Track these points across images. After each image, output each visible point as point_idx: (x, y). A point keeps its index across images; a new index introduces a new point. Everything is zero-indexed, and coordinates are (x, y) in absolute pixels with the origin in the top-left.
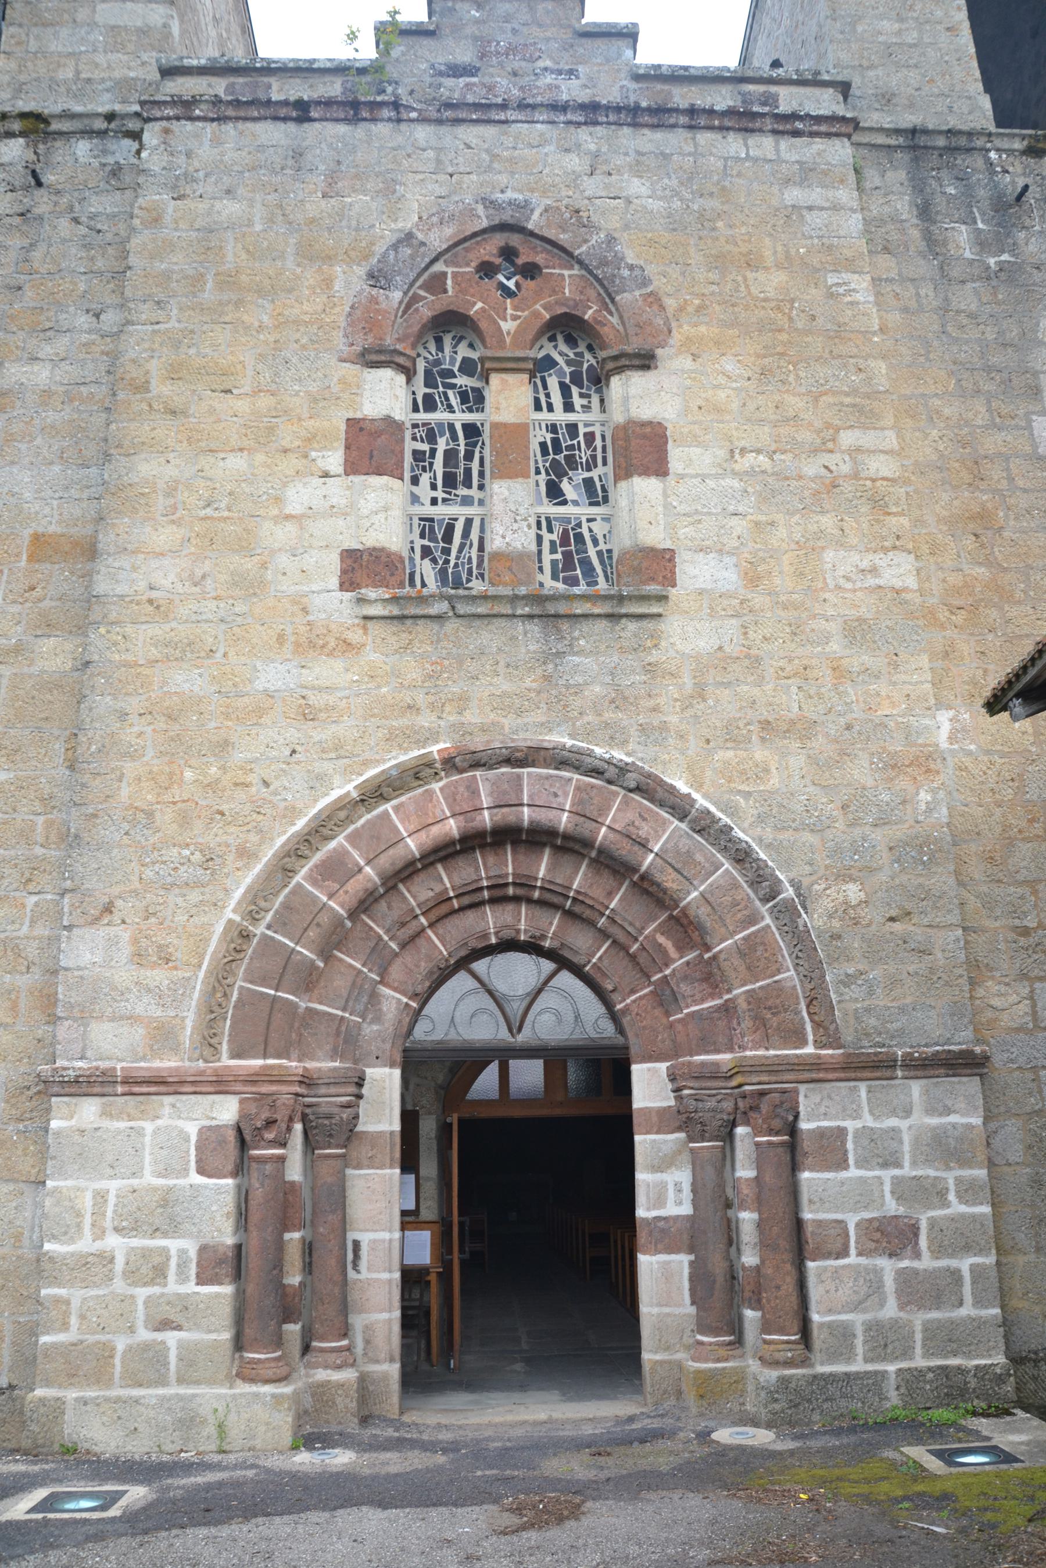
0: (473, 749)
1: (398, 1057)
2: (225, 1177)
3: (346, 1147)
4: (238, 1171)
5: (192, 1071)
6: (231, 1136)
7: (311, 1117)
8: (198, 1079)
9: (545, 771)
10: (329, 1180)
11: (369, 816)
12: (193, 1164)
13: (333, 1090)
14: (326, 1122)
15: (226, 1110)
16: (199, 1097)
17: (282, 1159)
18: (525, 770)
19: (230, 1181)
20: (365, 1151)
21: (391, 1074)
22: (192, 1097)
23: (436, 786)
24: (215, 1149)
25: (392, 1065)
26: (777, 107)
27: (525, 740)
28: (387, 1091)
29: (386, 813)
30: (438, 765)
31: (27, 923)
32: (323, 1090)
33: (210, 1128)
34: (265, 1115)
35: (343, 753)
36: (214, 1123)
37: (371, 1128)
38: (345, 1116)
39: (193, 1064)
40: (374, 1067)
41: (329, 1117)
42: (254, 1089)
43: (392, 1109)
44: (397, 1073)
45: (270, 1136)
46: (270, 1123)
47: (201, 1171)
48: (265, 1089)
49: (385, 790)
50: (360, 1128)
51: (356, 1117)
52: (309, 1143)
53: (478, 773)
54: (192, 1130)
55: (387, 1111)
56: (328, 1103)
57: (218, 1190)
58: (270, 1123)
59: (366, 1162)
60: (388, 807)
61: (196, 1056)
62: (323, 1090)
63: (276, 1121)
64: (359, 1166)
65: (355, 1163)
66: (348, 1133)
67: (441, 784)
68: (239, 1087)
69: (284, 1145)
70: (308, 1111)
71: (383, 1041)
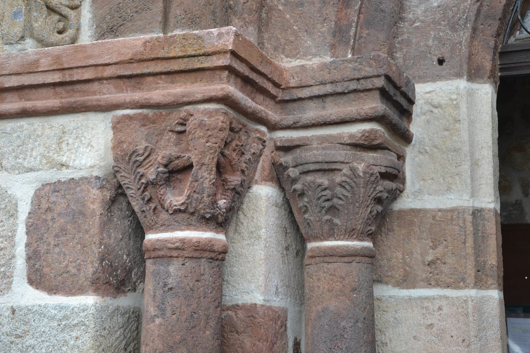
1: (486, 60)
2: (81, 291)
3: (372, 236)
4: (119, 277)
5: (12, 66)
6: (95, 199)
7: (293, 172)
8: (27, 80)
10: (333, 305)
12: (20, 264)
13: (333, 110)
14: (323, 180)
15: (86, 146)
16: (36, 123)
17: (218, 257)
19: (89, 300)
20: (418, 250)
21: (470, 94)
22: (24, 123)
24: (63, 230)
25: (473, 75)
28: (464, 127)
31: (159, 85)
32: (312, 112)
33: (56, 187)
34: (167, 149)
36: (65, 175)
37: (430, 202)
38: (361, 167)
39: (14, 50)
40: (436, 78)
41: (327, 168)
42: (138, 96)
43: (475, 164)
44: (486, 93)
45: (175, 198)
46: (176, 172)
47: (37, 280)
48: (161, 92)
50: (406, 202)
51: (394, 175)
52: (296, 233)
54: (23, 191)
55: (466, 167)
56: (323, 139)
57: (66, 321)
58: (176, 172)
59: (422, 273)
61: (17, 30)
62: (312, 112)
63: (191, 166)
64: (407, 281)
65: (398, 274)
66: (381, 208)
68: (109, 94)
69: (221, 221)
70: (286, 159)
71: (453, 28)
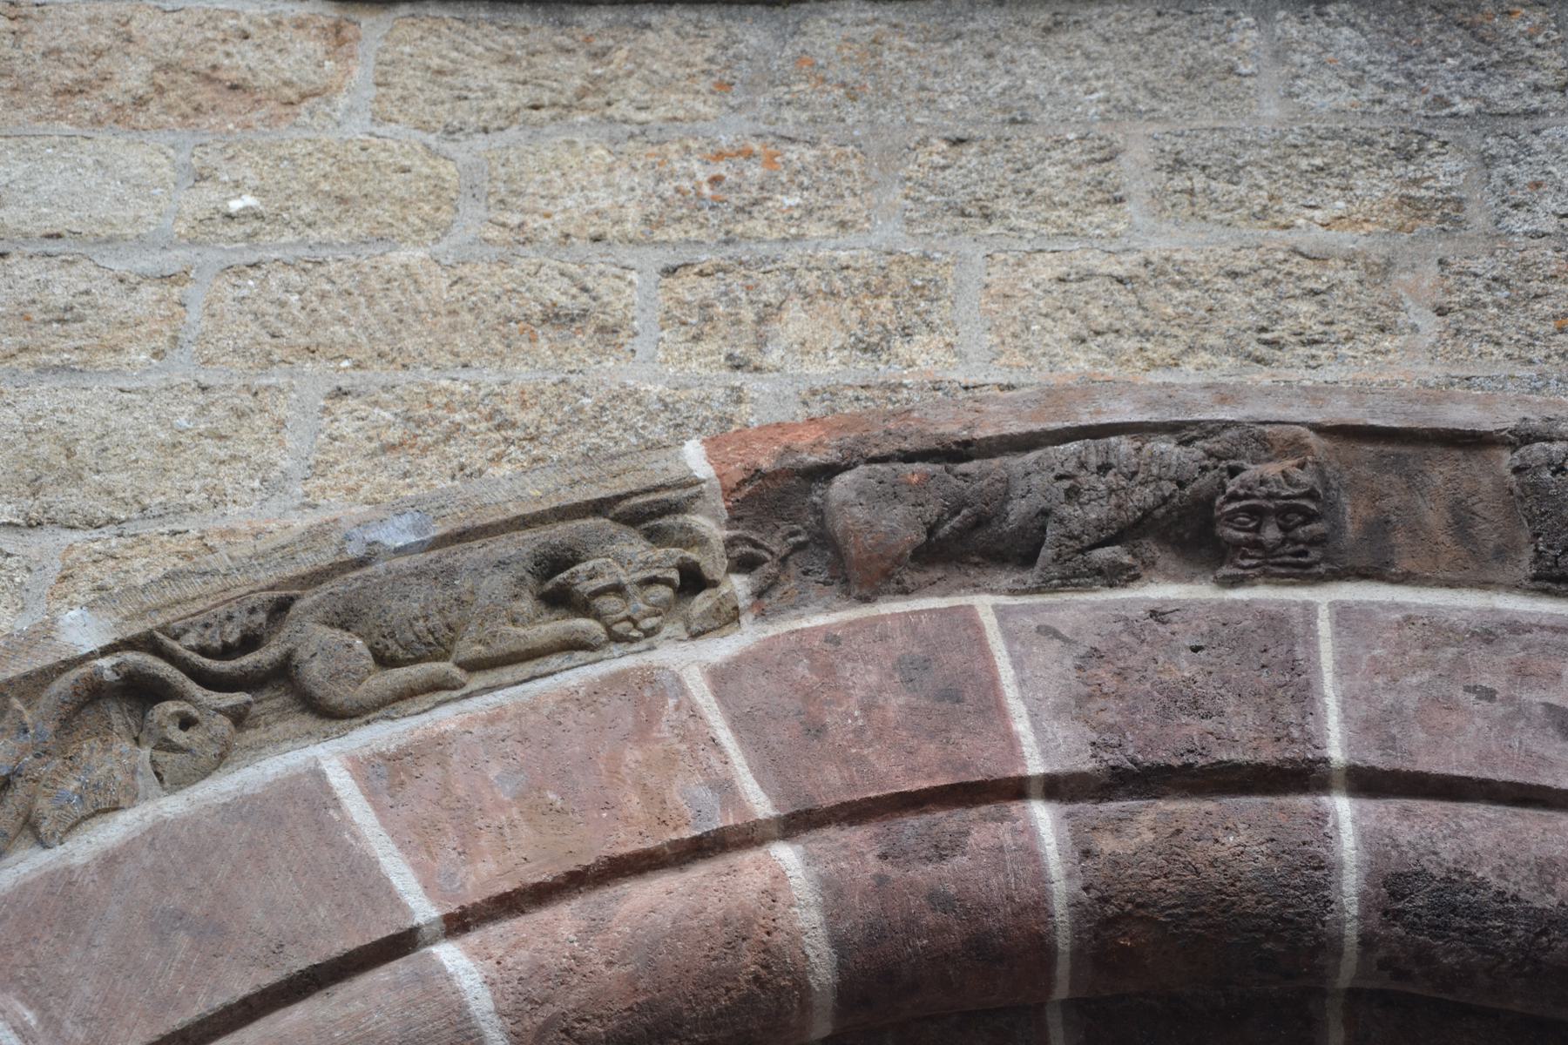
0: (951, 427)
9: (1466, 603)
11: (173, 806)
18: (1324, 597)
23: (688, 661)
26: (1415, 762)
27: (1314, 394)
29: (313, 795)
30: (710, 524)
35: (72, 499)
49: (316, 644)
53: (984, 605)
60: (333, 757)
67: (722, 648)
